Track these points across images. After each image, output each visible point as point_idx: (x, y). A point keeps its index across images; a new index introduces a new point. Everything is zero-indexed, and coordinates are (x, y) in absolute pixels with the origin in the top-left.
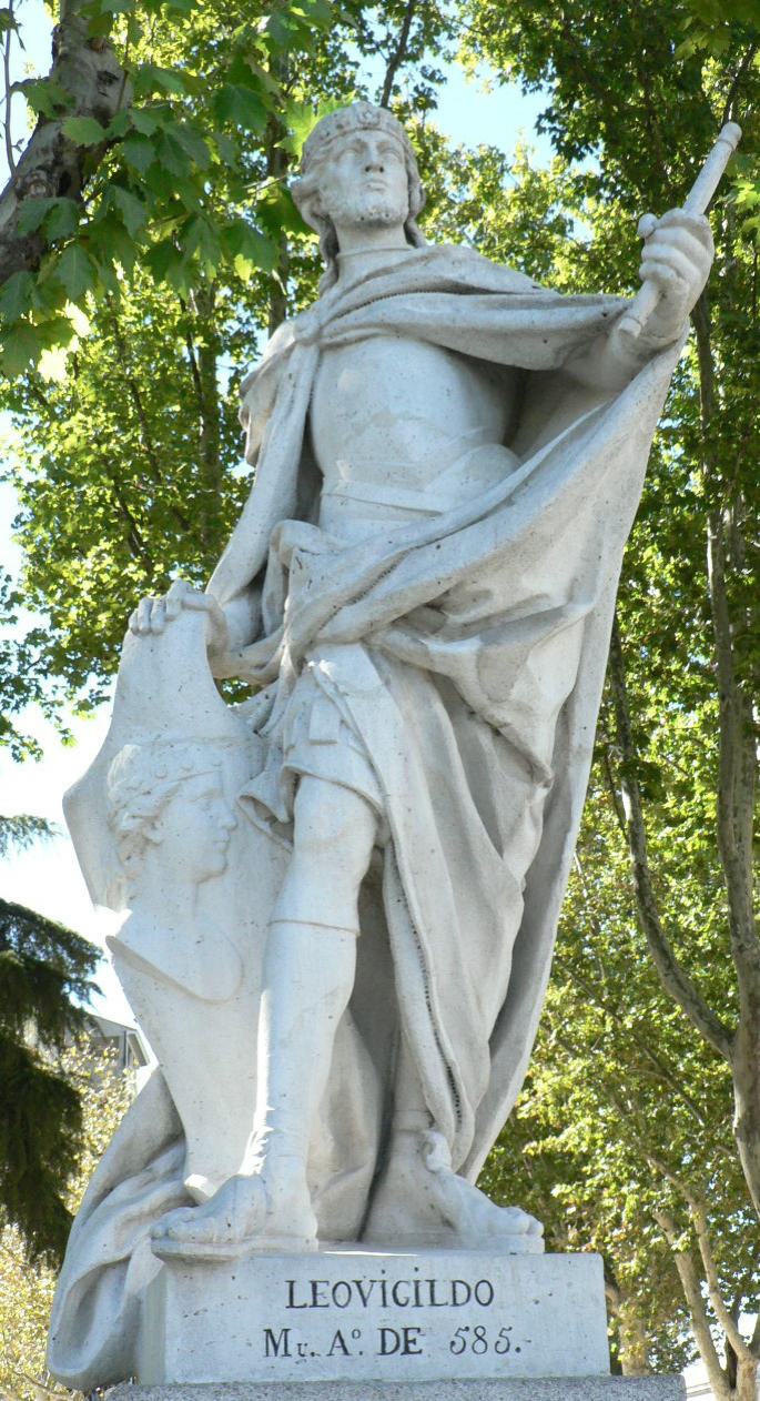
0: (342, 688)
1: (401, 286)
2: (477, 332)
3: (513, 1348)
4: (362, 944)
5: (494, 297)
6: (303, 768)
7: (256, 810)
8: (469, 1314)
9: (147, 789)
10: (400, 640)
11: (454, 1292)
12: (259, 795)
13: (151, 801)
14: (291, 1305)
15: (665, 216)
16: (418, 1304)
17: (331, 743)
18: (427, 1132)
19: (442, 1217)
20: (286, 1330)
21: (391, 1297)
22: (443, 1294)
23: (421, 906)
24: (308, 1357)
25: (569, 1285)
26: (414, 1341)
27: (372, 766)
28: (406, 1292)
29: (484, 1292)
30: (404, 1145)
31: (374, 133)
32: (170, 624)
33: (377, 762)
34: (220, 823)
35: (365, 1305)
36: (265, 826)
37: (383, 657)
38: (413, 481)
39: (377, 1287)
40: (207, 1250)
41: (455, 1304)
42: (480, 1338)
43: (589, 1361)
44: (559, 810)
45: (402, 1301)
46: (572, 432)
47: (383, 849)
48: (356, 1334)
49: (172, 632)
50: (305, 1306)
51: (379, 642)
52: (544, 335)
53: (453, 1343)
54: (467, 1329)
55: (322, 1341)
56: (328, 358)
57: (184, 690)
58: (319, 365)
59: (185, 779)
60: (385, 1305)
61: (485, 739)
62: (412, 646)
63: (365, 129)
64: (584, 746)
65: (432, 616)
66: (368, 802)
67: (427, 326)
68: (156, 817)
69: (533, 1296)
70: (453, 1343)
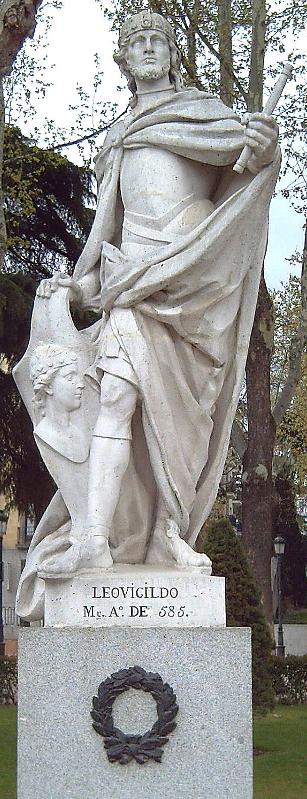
3: (185, 615)
4: (133, 443)
7: (92, 381)
8: (166, 602)
9: (45, 372)
10: (146, 307)
11: (161, 592)
12: (90, 374)
13: (45, 377)
16: (146, 597)
21: (135, 594)
22: (157, 593)
26: (144, 611)
29: (174, 593)
30: (160, 524)
35: (125, 597)
38: (157, 225)
39: (130, 590)
40: (66, 576)
41: (162, 597)
42: (171, 610)
44: (232, 375)
45: (140, 596)
47: (139, 406)
50: (100, 597)
52: (218, 153)
53: (160, 612)
54: (166, 607)
55: (107, 611)
56: (127, 154)
58: (123, 157)
60: (133, 597)
61: (188, 350)
68: (50, 384)
70: (160, 612)
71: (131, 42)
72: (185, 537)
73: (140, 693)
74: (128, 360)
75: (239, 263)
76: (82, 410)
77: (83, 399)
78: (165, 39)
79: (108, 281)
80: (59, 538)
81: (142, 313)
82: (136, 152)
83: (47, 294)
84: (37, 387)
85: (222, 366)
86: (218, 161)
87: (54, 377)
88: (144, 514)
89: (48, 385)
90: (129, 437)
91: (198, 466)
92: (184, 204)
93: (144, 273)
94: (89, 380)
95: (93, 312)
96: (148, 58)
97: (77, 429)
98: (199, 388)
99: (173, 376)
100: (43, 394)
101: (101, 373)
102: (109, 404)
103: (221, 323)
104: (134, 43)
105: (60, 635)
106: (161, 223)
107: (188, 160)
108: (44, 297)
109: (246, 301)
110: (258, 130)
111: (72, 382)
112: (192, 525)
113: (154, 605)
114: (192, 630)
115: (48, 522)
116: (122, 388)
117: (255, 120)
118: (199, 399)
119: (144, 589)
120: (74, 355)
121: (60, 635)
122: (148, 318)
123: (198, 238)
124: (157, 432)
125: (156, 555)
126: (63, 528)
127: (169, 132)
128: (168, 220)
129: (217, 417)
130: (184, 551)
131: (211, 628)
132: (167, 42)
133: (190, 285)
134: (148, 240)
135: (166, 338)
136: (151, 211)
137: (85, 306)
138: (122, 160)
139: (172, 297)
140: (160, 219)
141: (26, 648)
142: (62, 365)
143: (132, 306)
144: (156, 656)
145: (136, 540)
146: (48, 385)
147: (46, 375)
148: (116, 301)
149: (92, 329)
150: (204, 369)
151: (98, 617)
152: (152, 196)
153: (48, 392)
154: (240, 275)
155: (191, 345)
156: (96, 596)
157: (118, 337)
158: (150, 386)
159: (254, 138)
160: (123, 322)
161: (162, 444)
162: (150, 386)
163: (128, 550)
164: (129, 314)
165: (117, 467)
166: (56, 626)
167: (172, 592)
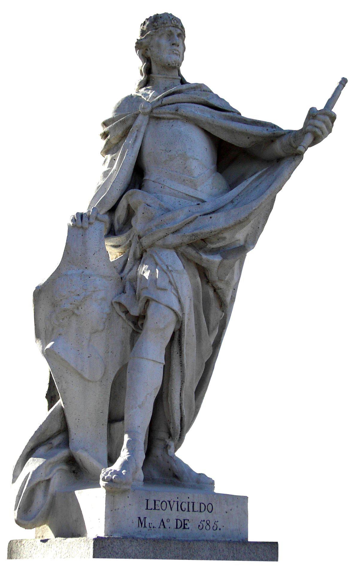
0: (170, 268)
1: (189, 100)
2: (222, 128)
3: (218, 529)
5: (228, 114)
6: (150, 296)
8: (203, 516)
9: (78, 293)
10: (191, 252)
12: (123, 302)
14: (147, 509)
17: (166, 290)
18: (167, 441)
19: (174, 474)
20: (145, 518)
21: (180, 508)
22: (197, 508)
24: (152, 528)
25: (237, 507)
27: (180, 301)
28: (185, 506)
29: (210, 507)
33: (182, 299)
34: (105, 311)
36: (123, 315)
37: (184, 257)
39: (176, 503)
41: (200, 511)
42: (208, 524)
45: (184, 509)
49: (91, 229)
51: (181, 250)
52: (248, 135)
53: (199, 526)
60: (178, 510)
61: (211, 293)
62: (196, 255)
65: (202, 243)
66: (175, 313)
67: (201, 121)
69: (225, 510)
70: (199, 526)
156: (149, 508)
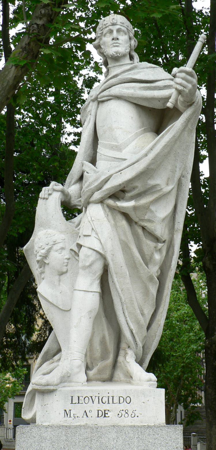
0: (93, 219)
3: (124, 411)
8: (124, 406)
10: (111, 202)
11: (119, 400)
13: (43, 251)
14: (72, 403)
15: (180, 68)
18: (127, 349)
21: (101, 400)
22: (116, 400)
23: (119, 283)
24: (76, 418)
25: (154, 398)
26: (107, 414)
28: (105, 400)
29: (128, 400)
30: (122, 352)
31: (115, 26)
32: (50, 196)
35: (93, 403)
38: (118, 148)
39: (97, 398)
40: (52, 388)
42: (126, 413)
43: (159, 420)
44: (171, 249)
45: (104, 402)
46: (166, 132)
47: (106, 270)
48: (90, 411)
50: (76, 403)
53: (118, 414)
54: (123, 410)
55: (81, 413)
57: (53, 217)
58: (98, 107)
59: (54, 244)
60: (99, 403)
61: (140, 231)
63: (113, 25)
64: (179, 228)
65: (122, 194)
70: (118, 414)
71: (104, 33)
72: (140, 363)
73: (118, 359)
74: (97, 237)
75: (173, 172)
76: (68, 274)
77: (69, 267)
78: (127, 31)
79: (86, 185)
80: (53, 364)
81: (109, 207)
82: (106, 103)
83: (46, 196)
84: (39, 258)
85: (164, 242)
86: (158, 106)
87: (50, 251)
88: (111, 347)
89: (46, 256)
90: (98, 290)
91: (148, 312)
92: (137, 135)
93: (109, 179)
94: (73, 253)
95: (78, 208)
96: (114, 43)
97: (65, 287)
98: (148, 257)
99: (130, 249)
100: (42, 263)
101: (80, 246)
102: (85, 268)
103: (162, 211)
104: (106, 34)
105: (46, 430)
106: (121, 147)
107: (143, 108)
108: (44, 199)
109: (180, 199)
110: (183, 79)
111: (62, 255)
112: (144, 353)
113: (114, 409)
114: (141, 427)
115: (46, 353)
116: (93, 256)
117: (181, 72)
118: (148, 264)
119: (107, 397)
120: (63, 236)
121: (46, 430)
122: (112, 209)
123: (146, 155)
124: (118, 287)
125: (119, 374)
126: (56, 358)
127: (128, 88)
128: (126, 145)
129: (161, 278)
130: (139, 372)
131: (155, 426)
132: (127, 33)
133: (140, 186)
134: (113, 158)
135: (124, 223)
136: (116, 140)
137: (72, 205)
138: (97, 109)
139: (128, 195)
140: (121, 144)
141: (21, 440)
142: (55, 243)
143: (101, 201)
144: (114, 446)
145: (104, 363)
146: (46, 256)
147: (44, 250)
148: (91, 199)
149: (76, 220)
150: (151, 244)
151: (74, 418)
152: (115, 130)
153: (46, 262)
154: (174, 179)
155: (141, 228)
157: (91, 222)
158: (113, 255)
159: (180, 84)
160: (95, 215)
161: (122, 295)
162: (113, 255)
163: (100, 372)
164: (99, 206)
165: (90, 311)
166: (44, 424)
167: (127, 400)
